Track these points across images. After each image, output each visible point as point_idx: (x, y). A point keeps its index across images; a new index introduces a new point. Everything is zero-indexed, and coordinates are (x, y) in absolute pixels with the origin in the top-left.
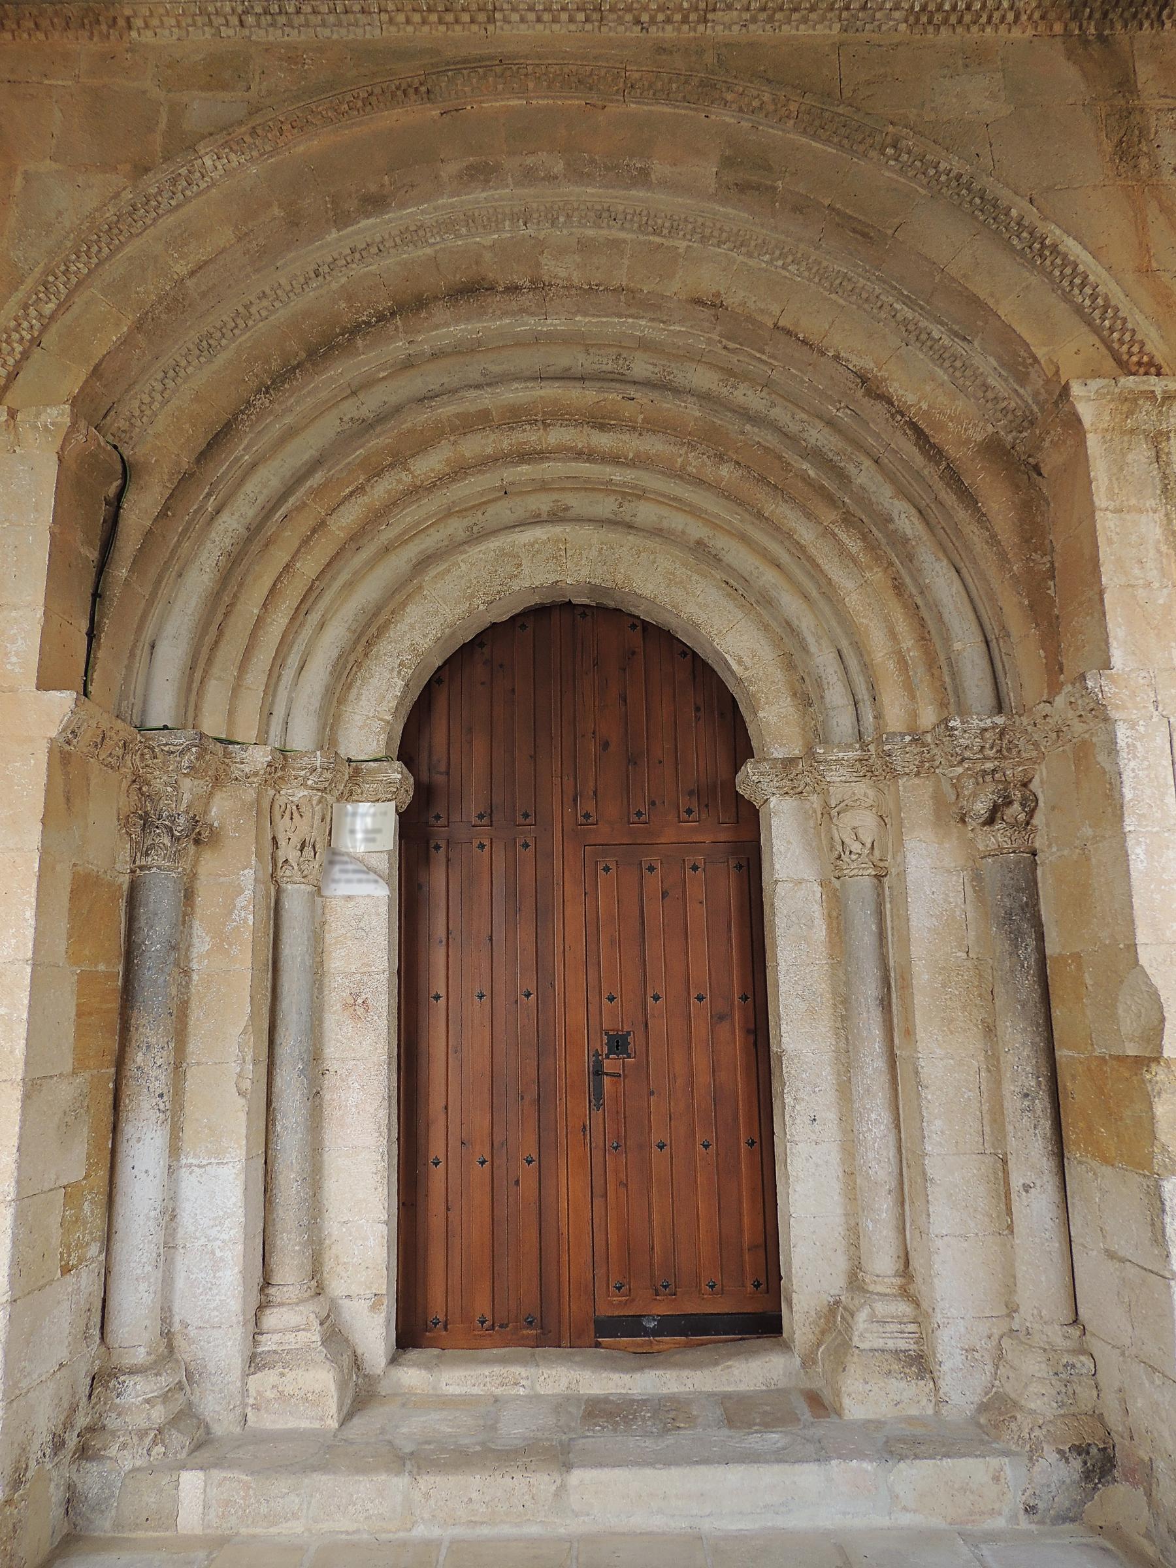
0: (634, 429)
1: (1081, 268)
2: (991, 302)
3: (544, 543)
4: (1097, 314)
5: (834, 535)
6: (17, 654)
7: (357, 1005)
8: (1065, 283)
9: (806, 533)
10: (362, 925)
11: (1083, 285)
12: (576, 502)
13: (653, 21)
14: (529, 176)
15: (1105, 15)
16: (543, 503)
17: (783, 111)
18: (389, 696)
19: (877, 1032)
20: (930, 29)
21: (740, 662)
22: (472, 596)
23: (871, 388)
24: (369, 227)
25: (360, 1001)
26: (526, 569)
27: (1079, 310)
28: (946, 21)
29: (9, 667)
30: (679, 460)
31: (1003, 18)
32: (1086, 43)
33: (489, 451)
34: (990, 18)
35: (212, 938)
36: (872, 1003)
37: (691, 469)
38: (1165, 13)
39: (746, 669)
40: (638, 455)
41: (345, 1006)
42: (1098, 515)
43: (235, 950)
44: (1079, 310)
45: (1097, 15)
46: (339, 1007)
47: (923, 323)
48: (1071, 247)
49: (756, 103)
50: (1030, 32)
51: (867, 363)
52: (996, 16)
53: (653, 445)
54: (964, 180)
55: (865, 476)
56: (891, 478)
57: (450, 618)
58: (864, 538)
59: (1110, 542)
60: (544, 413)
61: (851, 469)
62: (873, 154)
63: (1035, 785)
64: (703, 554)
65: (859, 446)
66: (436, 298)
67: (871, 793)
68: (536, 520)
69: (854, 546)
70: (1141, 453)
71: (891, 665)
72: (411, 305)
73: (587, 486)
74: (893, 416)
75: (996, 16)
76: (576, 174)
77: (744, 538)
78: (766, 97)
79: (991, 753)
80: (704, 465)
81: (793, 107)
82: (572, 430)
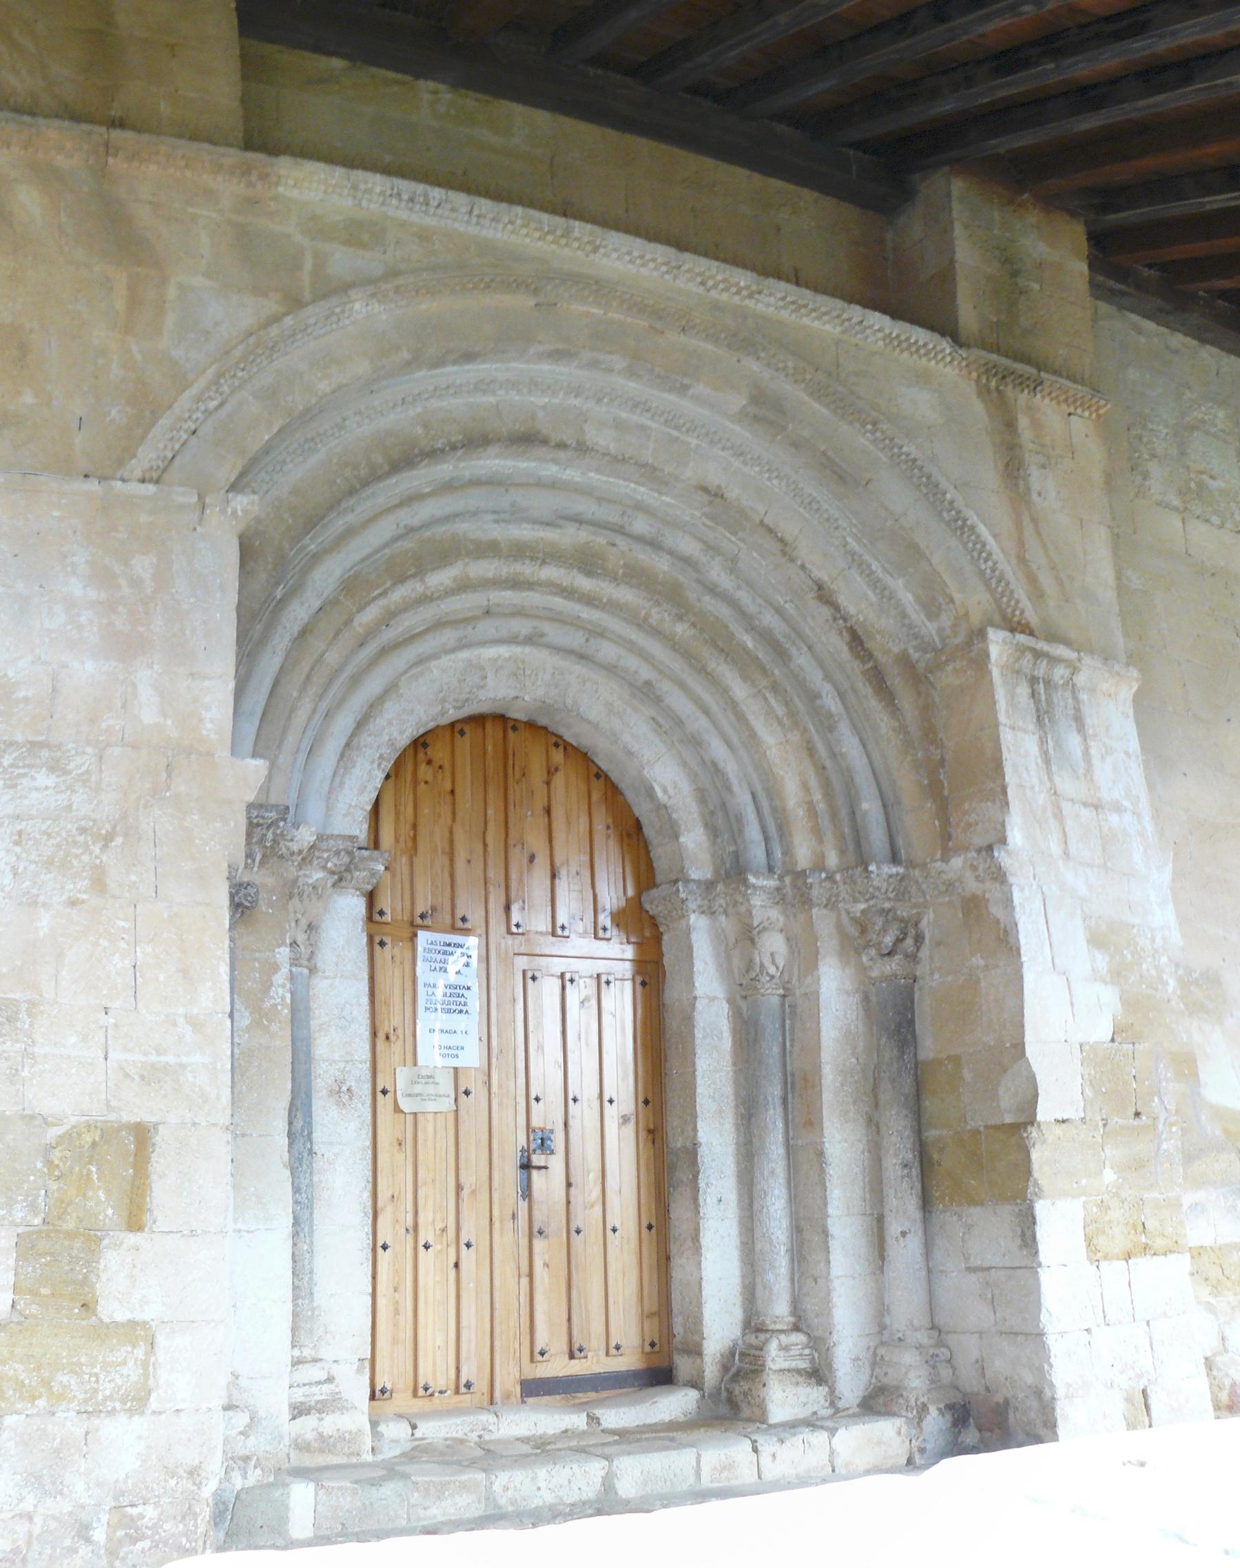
0: (615, 579)
1: (988, 547)
2: (928, 553)
3: (507, 660)
4: (994, 581)
5: (766, 699)
6: (212, 721)
7: (341, 1093)
8: (975, 554)
9: (740, 691)
10: (344, 1014)
11: (986, 560)
12: (553, 633)
13: (715, 286)
14: (594, 364)
15: (1004, 377)
16: (523, 627)
17: (800, 377)
18: (370, 787)
19: (780, 1124)
20: (898, 350)
21: (665, 791)
22: (444, 700)
23: (824, 594)
24: (452, 373)
25: (344, 1088)
26: (490, 681)
27: (982, 573)
28: (917, 351)
29: (204, 732)
30: (643, 612)
31: (943, 358)
32: (989, 391)
33: (490, 575)
34: (936, 355)
35: (251, 1013)
36: (778, 1102)
37: (653, 621)
38: (1039, 388)
39: (670, 797)
40: (610, 600)
41: (331, 1093)
42: (1001, 728)
43: (274, 1027)
44: (982, 573)
45: (1000, 376)
46: (324, 1093)
47: (867, 557)
48: (982, 529)
49: (781, 365)
50: (957, 371)
51: (823, 576)
52: (940, 356)
53: (626, 595)
54: (919, 463)
55: (802, 659)
56: (821, 664)
57: (424, 718)
58: (787, 704)
59: (1009, 751)
60: (544, 553)
61: (794, 652)
62: (857, 425)
63: (924, 924)
64: (646, 693)
65: (800, 635)
66: (499, 440)
67: (782, 919)
68: (513, 640)
69: (780, 710)
70: (1023, 690)
71: (801, 812)
72: (475, 440)
73: (557, 618)
74: (835, 619)
75: (940, 356)
76: (631, 373)
77: (683, 686)
78: (790, 364)
79: (892, 895)
80: (663, 620)
81: (808, 377)
82: (562, 571)
